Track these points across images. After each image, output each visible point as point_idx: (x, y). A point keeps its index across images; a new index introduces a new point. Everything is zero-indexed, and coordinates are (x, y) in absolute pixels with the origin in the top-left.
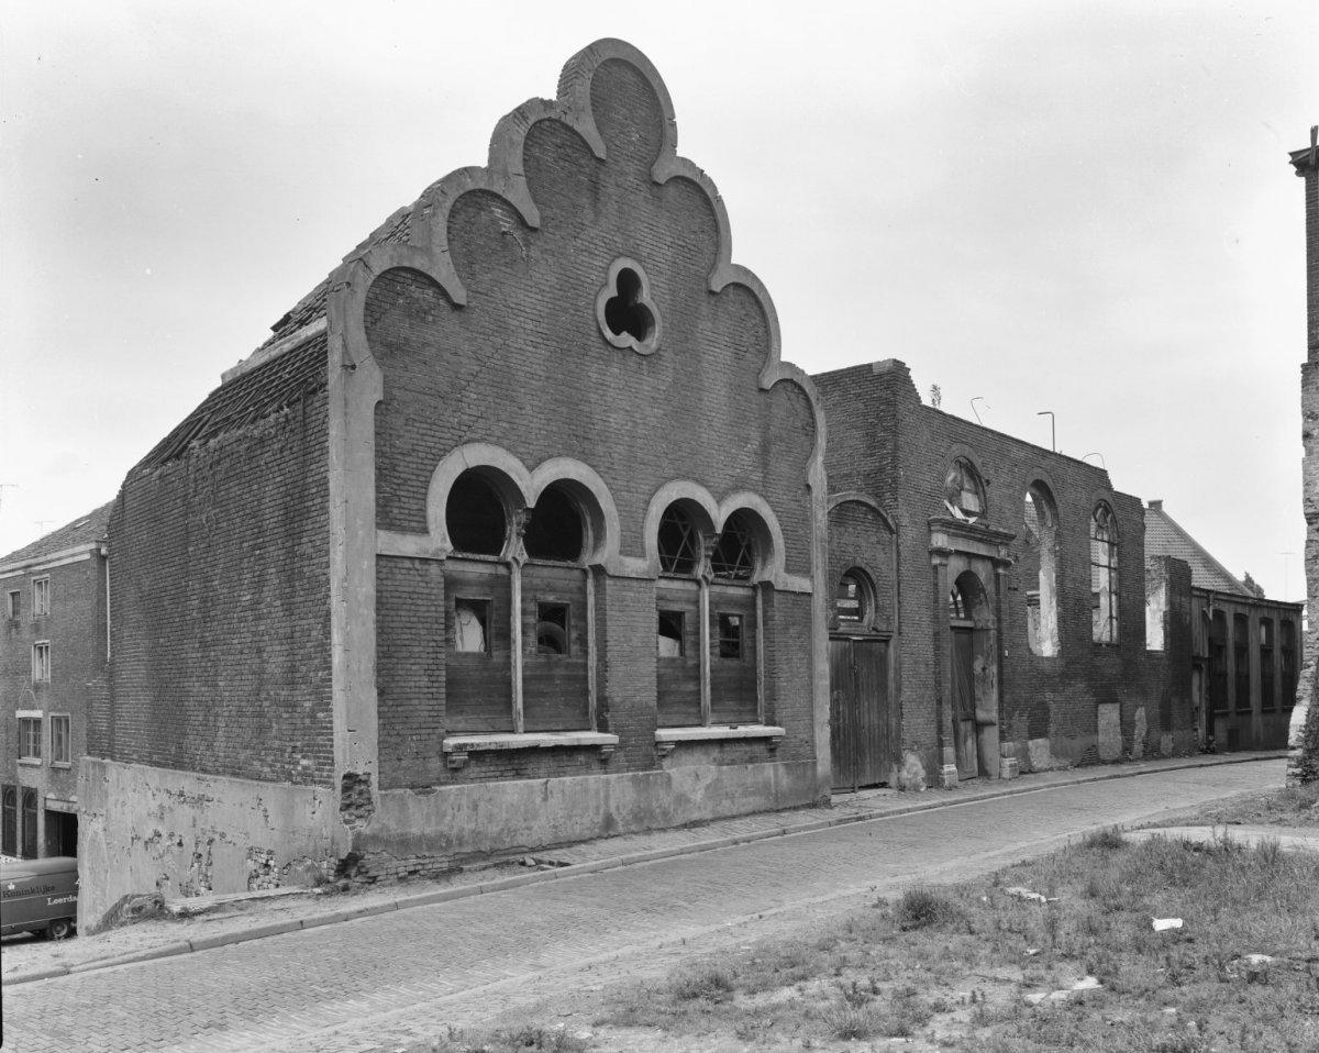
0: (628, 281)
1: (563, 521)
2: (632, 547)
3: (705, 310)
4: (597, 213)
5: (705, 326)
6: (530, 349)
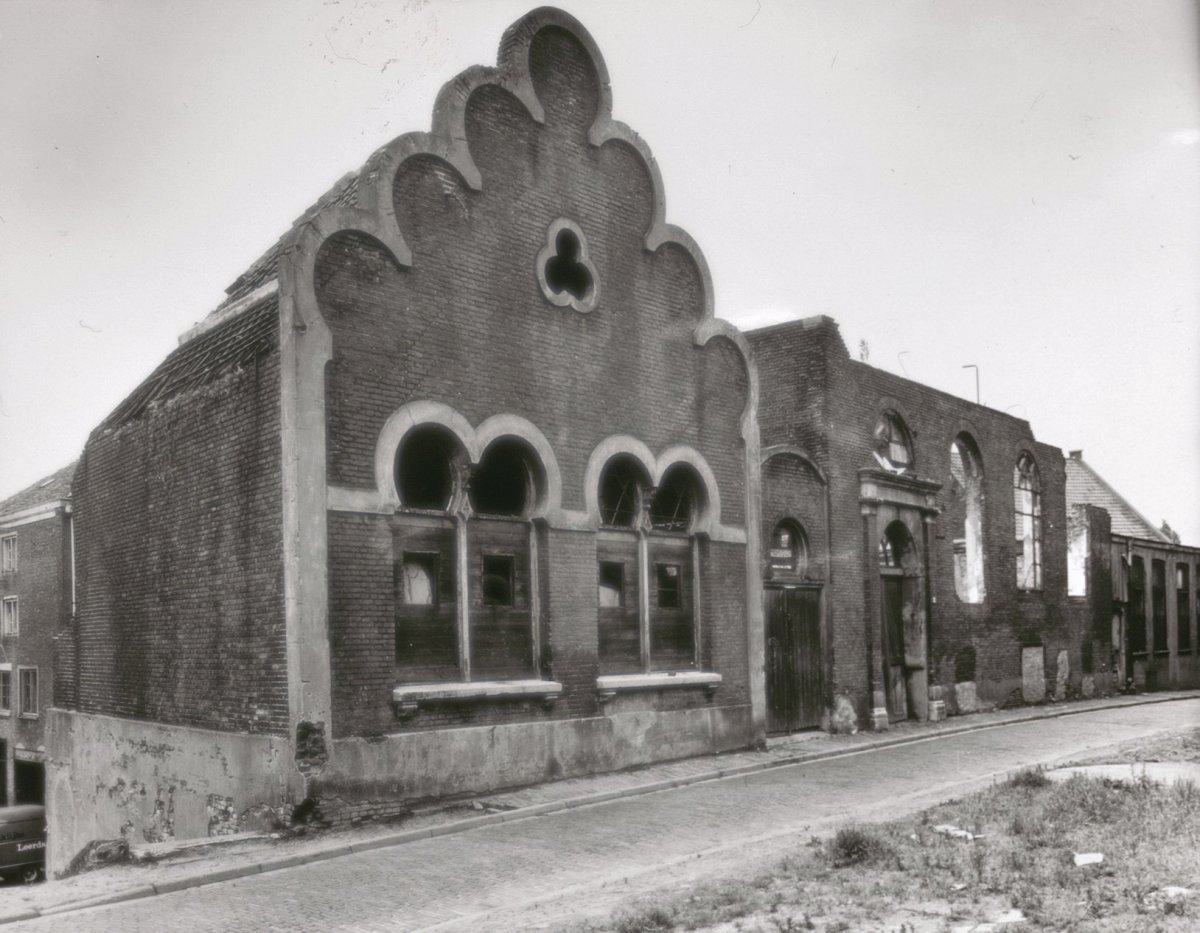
0: (567, 243)
1: (508, 476)
2: (573, 499)
3: (641, 268)
4: (536, 175)
5: (641, 284)
6: (473, 308)
